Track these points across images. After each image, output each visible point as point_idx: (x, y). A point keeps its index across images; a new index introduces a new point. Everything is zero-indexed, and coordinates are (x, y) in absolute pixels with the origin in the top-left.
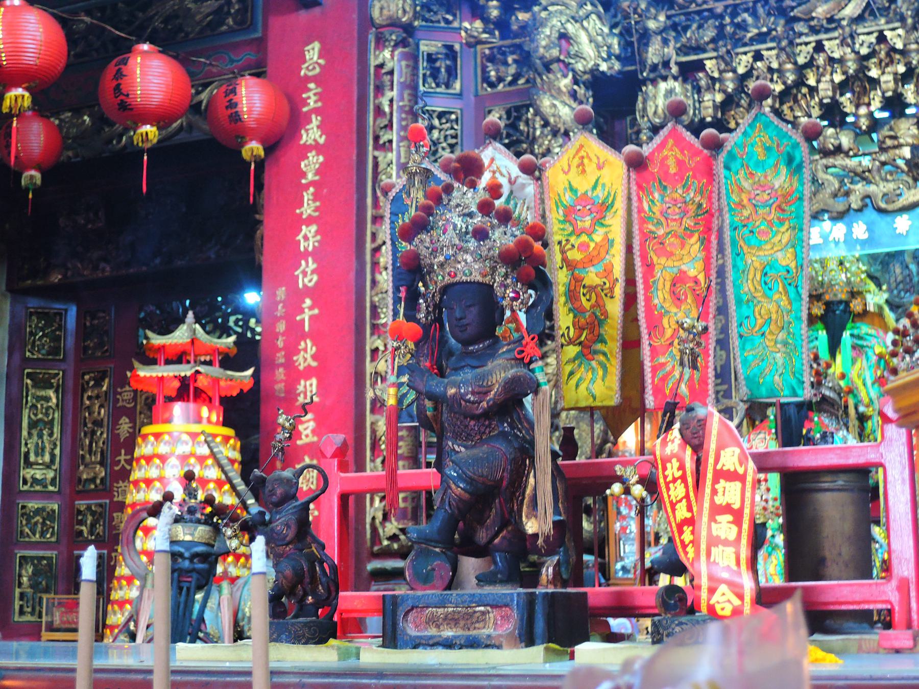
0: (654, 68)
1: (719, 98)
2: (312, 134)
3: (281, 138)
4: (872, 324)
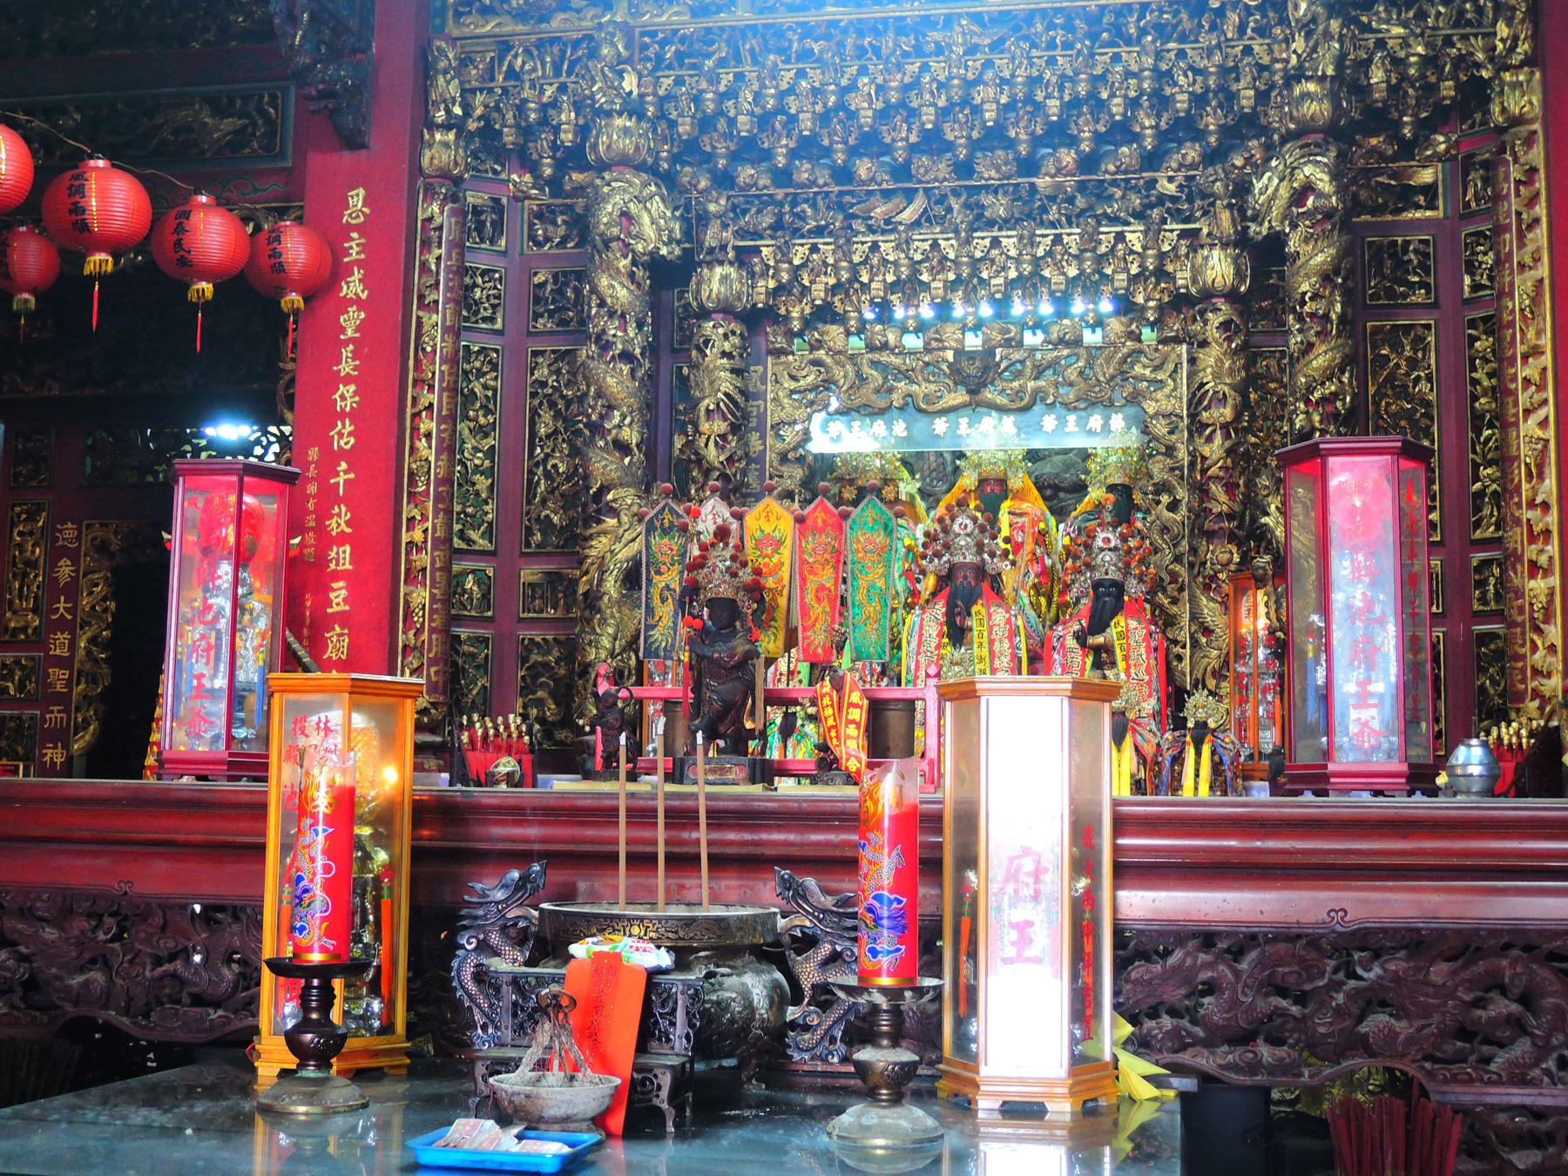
0: (711, 251)
1: (772, 284)
2: (353, 287)
3: (322, 287)
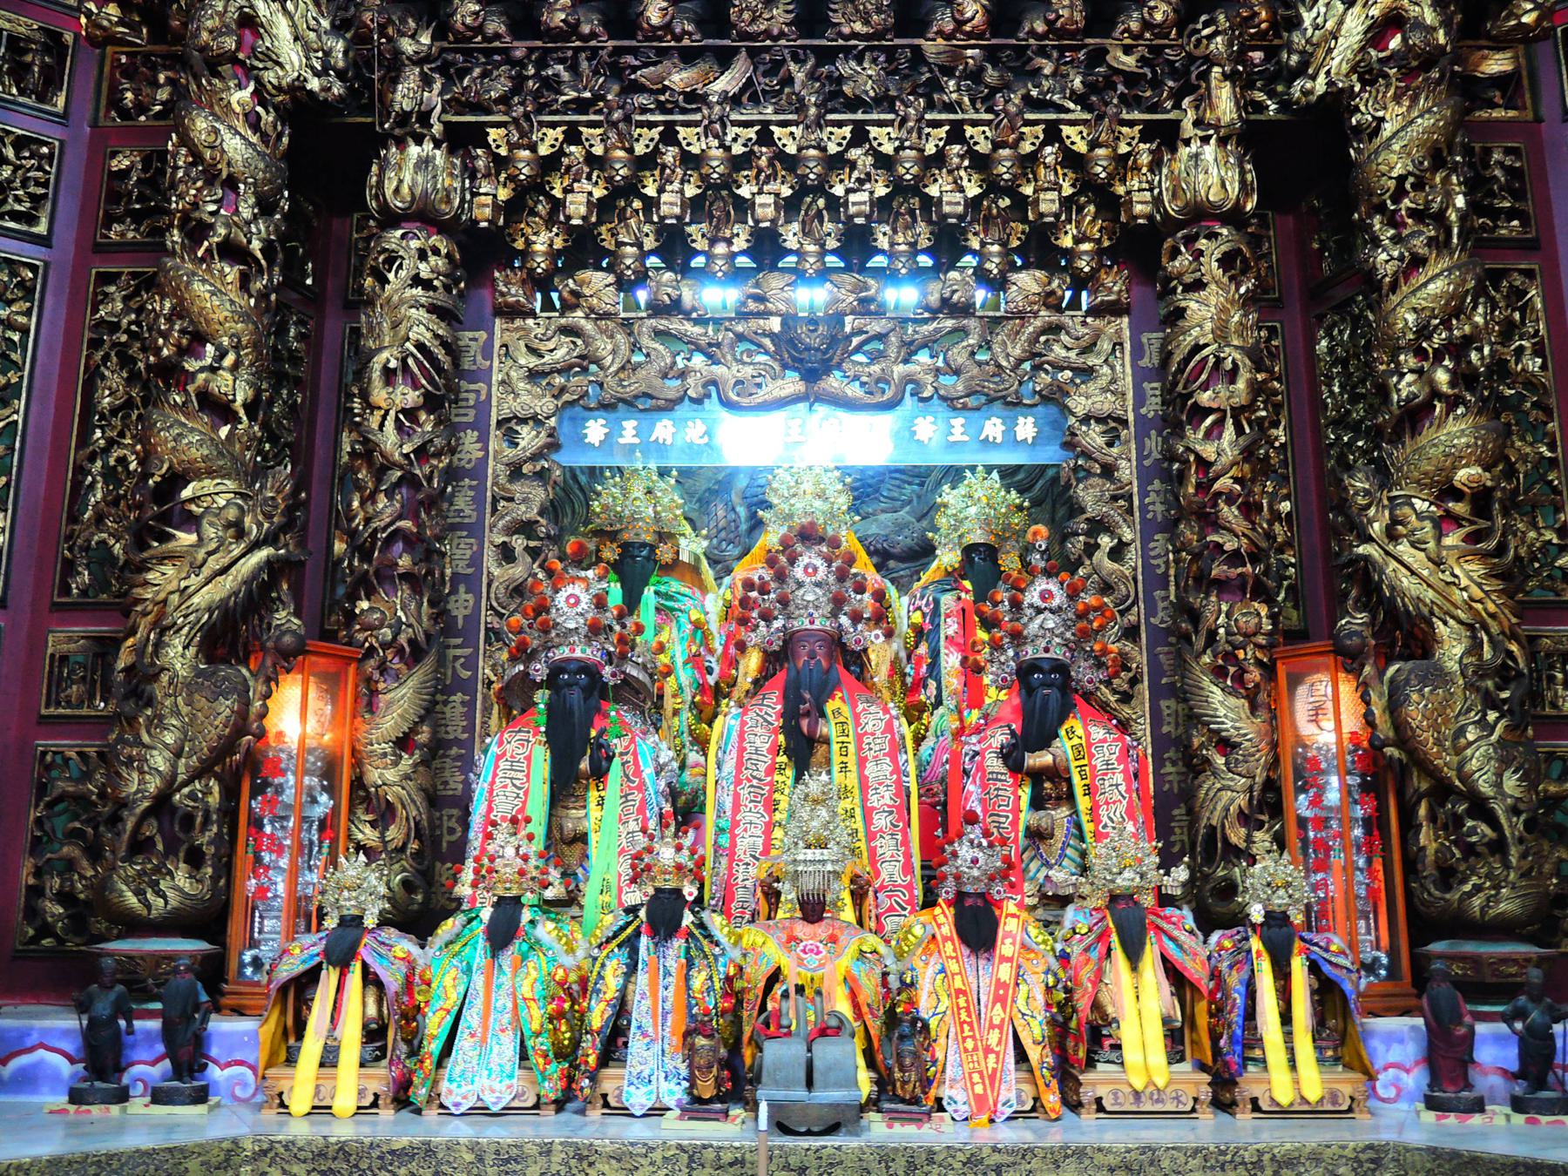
0: (404, 118)
4: (681, 579)
